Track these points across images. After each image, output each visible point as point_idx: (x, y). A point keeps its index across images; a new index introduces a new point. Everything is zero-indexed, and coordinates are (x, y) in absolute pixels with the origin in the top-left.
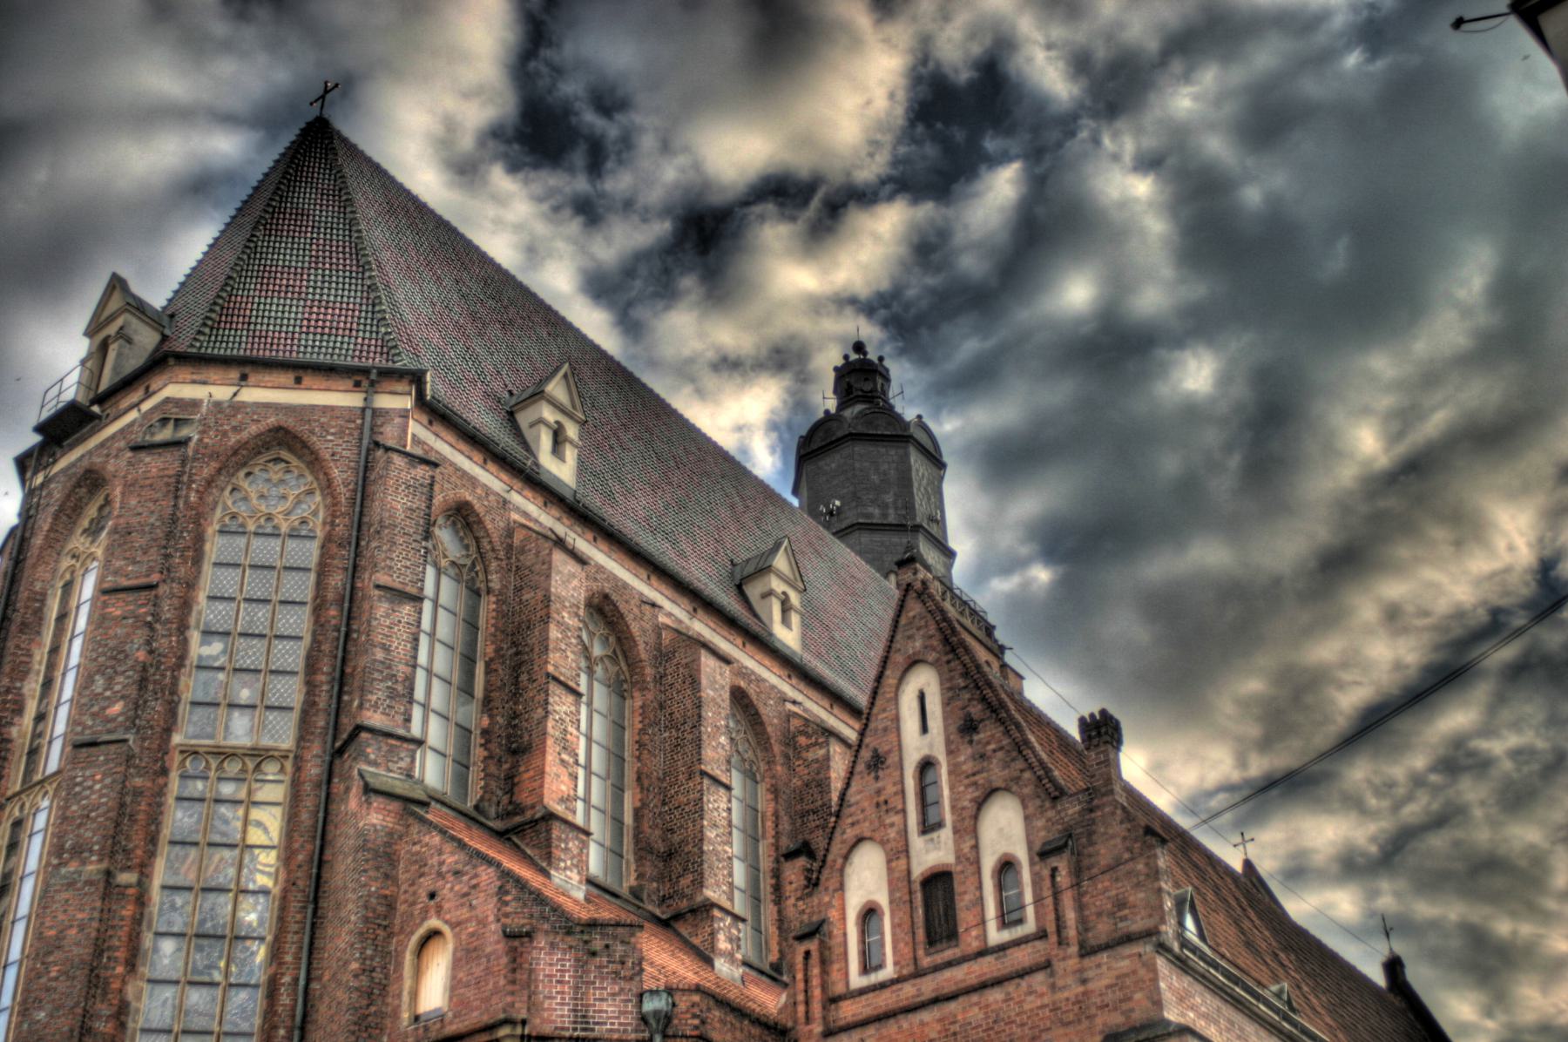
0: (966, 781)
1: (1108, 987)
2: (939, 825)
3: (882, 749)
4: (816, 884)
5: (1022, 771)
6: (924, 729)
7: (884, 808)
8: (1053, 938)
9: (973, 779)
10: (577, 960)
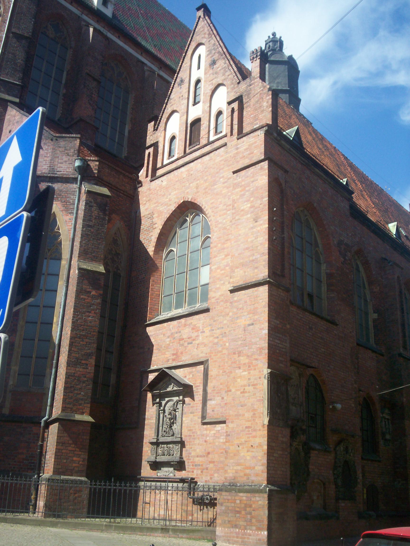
0: (209, 83)
1: (245, 150)
2: (199, 102)
4: (157, 130)
6: (199, 68)
7: (182, 98)
9: (211, 82)
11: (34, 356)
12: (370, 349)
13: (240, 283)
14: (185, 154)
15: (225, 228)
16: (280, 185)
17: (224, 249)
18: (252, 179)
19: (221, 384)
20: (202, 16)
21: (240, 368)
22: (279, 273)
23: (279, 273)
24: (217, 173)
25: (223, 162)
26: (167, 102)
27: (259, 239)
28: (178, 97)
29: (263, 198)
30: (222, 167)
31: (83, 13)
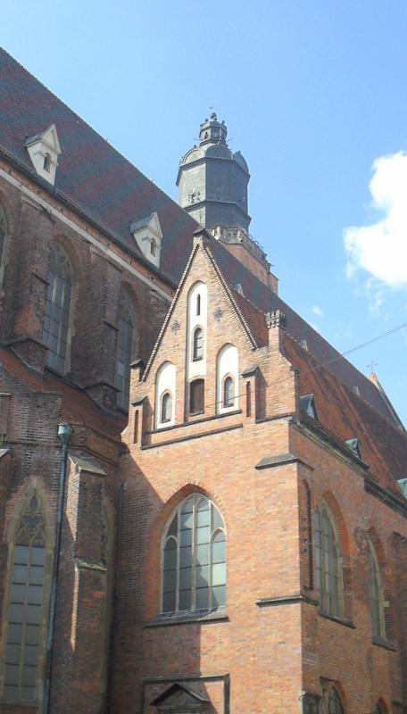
2: (201, 359)
3: (179, 321)
4: (144, 381)
5: (240, 336)
6: (199, 313)
8: (245, 413)
10: (31, 409)
11: (22, 664)
12: (382, 646)
13: (269, 596)
14: (186, 423)
15: (244, 527)
16: (307, 486)
17: (243, 550)
18: (279, 481)
19: (245, 702)
20: (201, 245)
21: (270, 687)
22: (308, 586)
23: (308, 586)
24: (232, 458)
25: (237, 447)
26: (158, 348)
27: (288, 550)
28: (171, 344)
29: (291, 504)
30: (237, 452)
31: (22, 184)
